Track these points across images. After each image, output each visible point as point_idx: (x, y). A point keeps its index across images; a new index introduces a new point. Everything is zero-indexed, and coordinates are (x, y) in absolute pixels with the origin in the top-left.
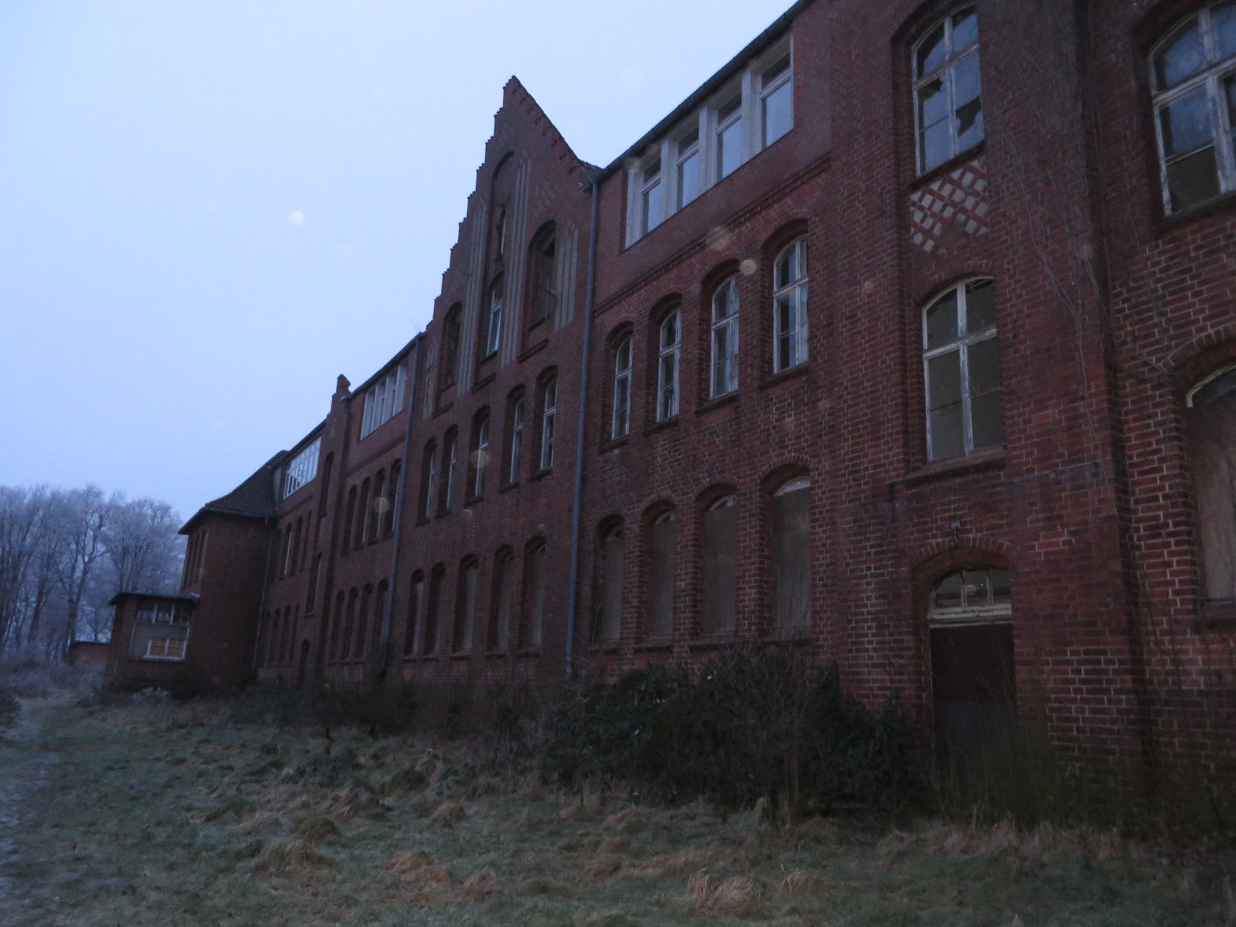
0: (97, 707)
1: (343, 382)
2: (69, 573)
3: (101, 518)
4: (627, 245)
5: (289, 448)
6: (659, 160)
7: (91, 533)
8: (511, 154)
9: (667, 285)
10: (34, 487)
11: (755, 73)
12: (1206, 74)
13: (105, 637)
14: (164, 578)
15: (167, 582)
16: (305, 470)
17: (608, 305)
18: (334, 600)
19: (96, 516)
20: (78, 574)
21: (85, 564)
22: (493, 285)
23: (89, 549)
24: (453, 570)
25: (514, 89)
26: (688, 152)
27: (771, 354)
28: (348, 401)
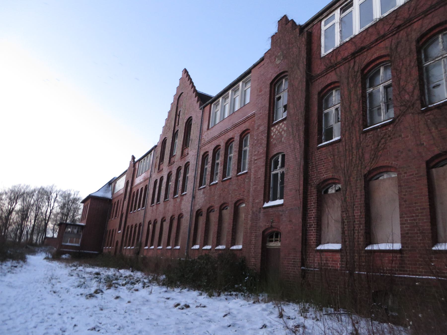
1: (133, 158)
3: (57, 195)
4: (246, 103)
7: (53, 200)
8: (182, 93)
9: (230, 135)
12: (78, 223)
13: (56, 236)
14: (77, 216)
15: (78, 217)
16: (120, 185)
17: (205, 145)
21: (51, 210)
22: (175, 135)
24: (217, 209)
25: (186, 71)
27: (241, 166)
28: (134, 163)
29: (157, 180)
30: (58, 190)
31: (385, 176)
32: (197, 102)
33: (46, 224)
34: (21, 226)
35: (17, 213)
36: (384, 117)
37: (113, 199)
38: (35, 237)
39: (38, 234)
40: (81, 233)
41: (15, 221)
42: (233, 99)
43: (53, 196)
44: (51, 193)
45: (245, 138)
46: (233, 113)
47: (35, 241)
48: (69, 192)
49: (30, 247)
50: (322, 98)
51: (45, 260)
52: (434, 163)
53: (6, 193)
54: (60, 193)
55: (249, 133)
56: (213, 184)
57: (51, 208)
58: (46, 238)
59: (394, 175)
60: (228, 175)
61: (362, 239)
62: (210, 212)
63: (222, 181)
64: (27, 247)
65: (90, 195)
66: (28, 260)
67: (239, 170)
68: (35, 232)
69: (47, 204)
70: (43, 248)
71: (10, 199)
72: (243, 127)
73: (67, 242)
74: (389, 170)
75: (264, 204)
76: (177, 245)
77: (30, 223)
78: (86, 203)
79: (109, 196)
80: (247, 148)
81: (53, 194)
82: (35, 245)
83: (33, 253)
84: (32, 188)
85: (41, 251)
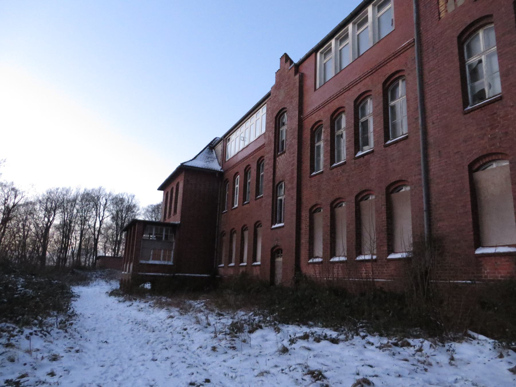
0: (75, 259)
1: (286, 58)
2: (93, 225)
3: (106, 200)
4: (327, 79)
5: (220, 135)
6: (348, 33)
7: (102, 207)
9: (336, 104)
11: (354, 24)
18: (305, 214)
19: (104, 199)
21: (101, 222)
23: (102, 214)
26: (344, 44)
30: (108, 193)
31: (494, 165)
32: (286, 62)
33: (96, 241)
34: (64, 246)
35: (57, 228)
36: (236, 206)
38: (83, 259)
39: (86, 255)
40: (174, 240)
42: (356, 37)
43: (102, 203)
45: (362, 105)
46: (340, 72)
47: (83, 264)
48: (121, 197)
49: (79, 272)
50: (463, 44)
53: (40, 202)
54: (110, 198)
55: (344, 111)
56: (336, 167)
57: (101, 218)
59: (506, 163)
64: (73, 273)
66: (77, 306)
69: (94, 213)
70: (100, 273)
71: (46, 209)
73: (148, 260)
75: (272, 226)
76: (231, 263)
79: (216, 166)
80: (322, 144)
81: (101, 200)
82: (84, 268)
84: (72, 195)
85: (96, 277)
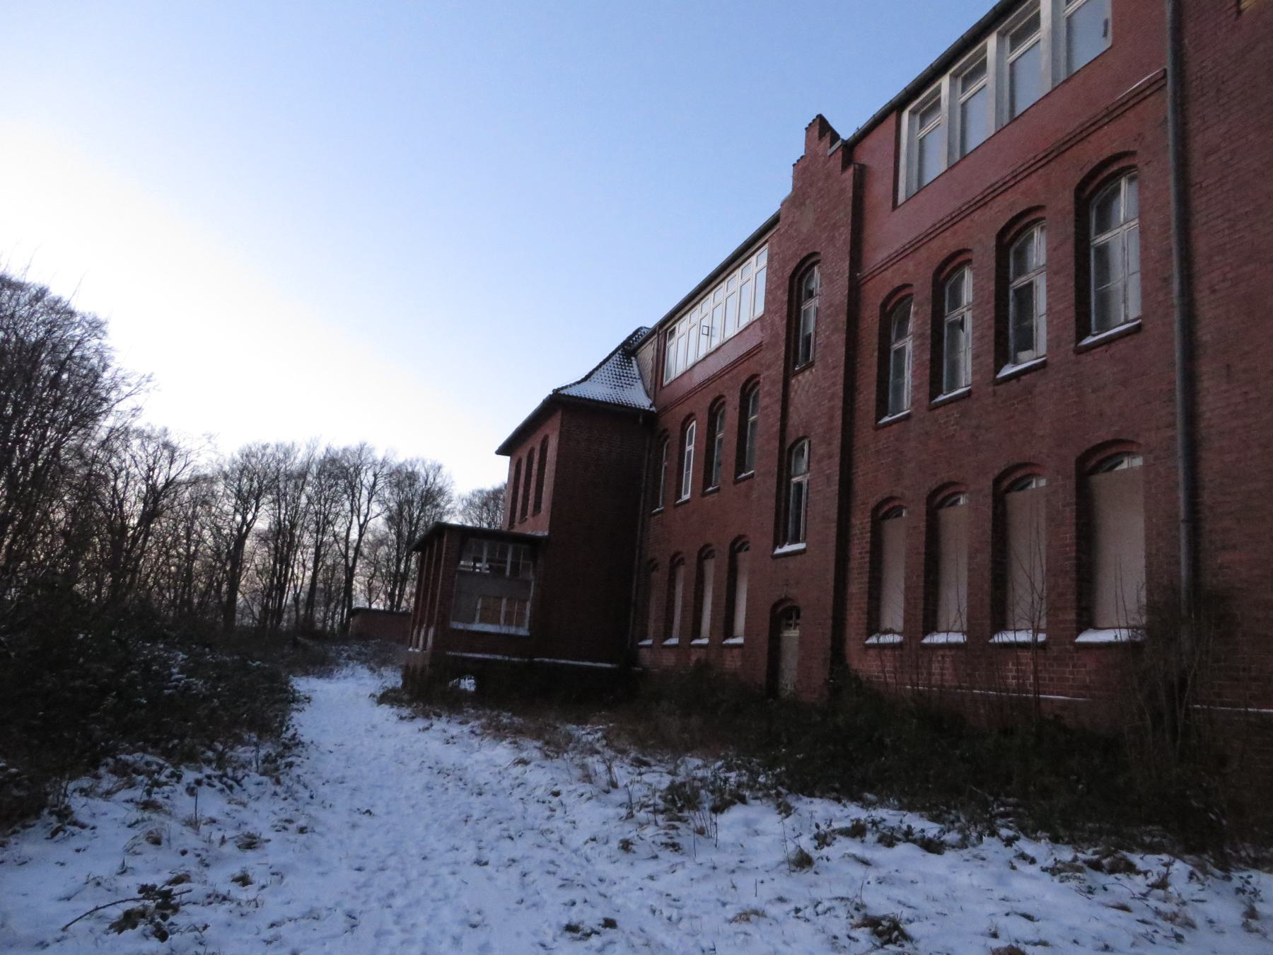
1: (821, 127)
3: (375, 475)
7: (365, 492)
10: (320, 453)
11: (1002, 35)
19: (370, 473)
20: (354, 535)
21: (361, 527)
23: (364, 509)
26: (974, 88)
29: (534, 515)
34: (278, 580)
35: (263, 538)
37: (665, 409)
38: (319, 615)
40: (531, 576)
41: (260, 567)
43: (365, 482)
44: (358, 471)
45: (1017, 244)
46: (961, 159)
48: (410, 470)
51: (386, 711)
52: (1093, 462)
53: (226, 477)
54: (385, 471)
56: (944, 403)
58: (354, 612)
60: (1104, 325)
61: (988, 622)
62: (739, 550)
63: (1080, 351)
64: (296, 644)
65: (556, 392)
67: (935, 389)
68: (319, 597)
69: (347, 506)
72: (1013, 202)
73: (472, 621)
74: (1134, 449)
77: (302, 574)
78: (523, 454)
79: (638, 397)
80: (909, 344)
81: (363, 476)
83: (322, 666)
